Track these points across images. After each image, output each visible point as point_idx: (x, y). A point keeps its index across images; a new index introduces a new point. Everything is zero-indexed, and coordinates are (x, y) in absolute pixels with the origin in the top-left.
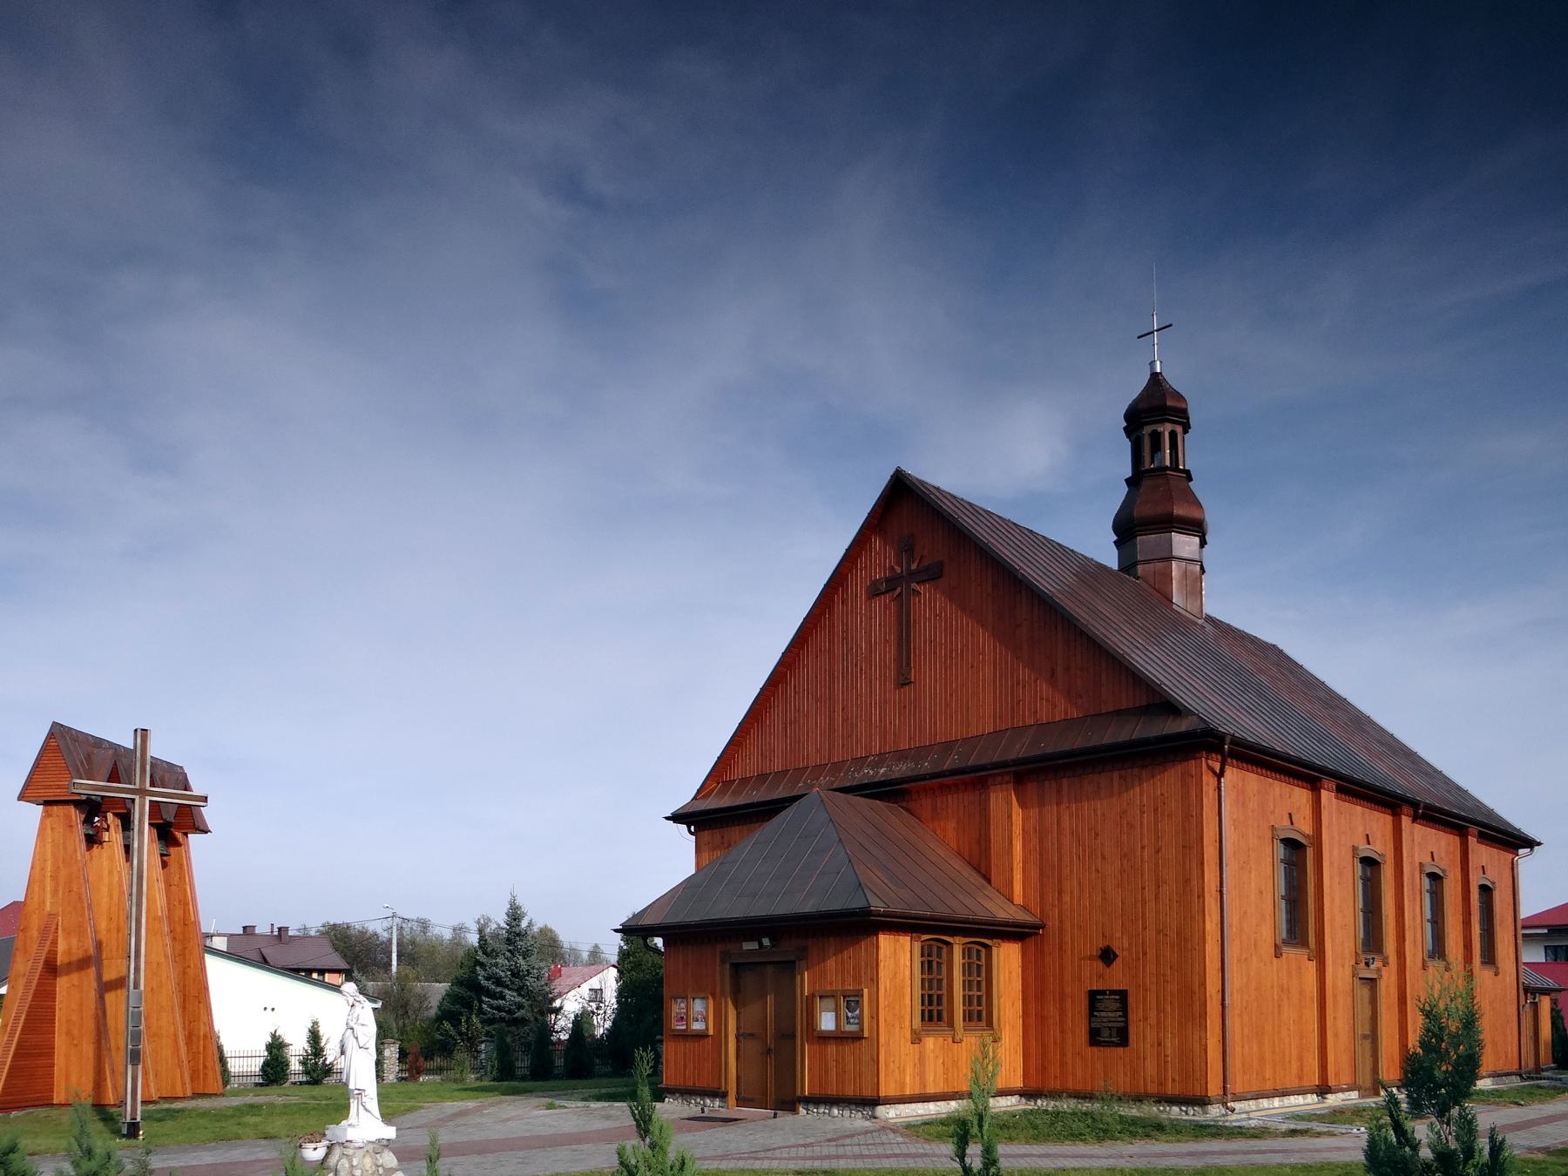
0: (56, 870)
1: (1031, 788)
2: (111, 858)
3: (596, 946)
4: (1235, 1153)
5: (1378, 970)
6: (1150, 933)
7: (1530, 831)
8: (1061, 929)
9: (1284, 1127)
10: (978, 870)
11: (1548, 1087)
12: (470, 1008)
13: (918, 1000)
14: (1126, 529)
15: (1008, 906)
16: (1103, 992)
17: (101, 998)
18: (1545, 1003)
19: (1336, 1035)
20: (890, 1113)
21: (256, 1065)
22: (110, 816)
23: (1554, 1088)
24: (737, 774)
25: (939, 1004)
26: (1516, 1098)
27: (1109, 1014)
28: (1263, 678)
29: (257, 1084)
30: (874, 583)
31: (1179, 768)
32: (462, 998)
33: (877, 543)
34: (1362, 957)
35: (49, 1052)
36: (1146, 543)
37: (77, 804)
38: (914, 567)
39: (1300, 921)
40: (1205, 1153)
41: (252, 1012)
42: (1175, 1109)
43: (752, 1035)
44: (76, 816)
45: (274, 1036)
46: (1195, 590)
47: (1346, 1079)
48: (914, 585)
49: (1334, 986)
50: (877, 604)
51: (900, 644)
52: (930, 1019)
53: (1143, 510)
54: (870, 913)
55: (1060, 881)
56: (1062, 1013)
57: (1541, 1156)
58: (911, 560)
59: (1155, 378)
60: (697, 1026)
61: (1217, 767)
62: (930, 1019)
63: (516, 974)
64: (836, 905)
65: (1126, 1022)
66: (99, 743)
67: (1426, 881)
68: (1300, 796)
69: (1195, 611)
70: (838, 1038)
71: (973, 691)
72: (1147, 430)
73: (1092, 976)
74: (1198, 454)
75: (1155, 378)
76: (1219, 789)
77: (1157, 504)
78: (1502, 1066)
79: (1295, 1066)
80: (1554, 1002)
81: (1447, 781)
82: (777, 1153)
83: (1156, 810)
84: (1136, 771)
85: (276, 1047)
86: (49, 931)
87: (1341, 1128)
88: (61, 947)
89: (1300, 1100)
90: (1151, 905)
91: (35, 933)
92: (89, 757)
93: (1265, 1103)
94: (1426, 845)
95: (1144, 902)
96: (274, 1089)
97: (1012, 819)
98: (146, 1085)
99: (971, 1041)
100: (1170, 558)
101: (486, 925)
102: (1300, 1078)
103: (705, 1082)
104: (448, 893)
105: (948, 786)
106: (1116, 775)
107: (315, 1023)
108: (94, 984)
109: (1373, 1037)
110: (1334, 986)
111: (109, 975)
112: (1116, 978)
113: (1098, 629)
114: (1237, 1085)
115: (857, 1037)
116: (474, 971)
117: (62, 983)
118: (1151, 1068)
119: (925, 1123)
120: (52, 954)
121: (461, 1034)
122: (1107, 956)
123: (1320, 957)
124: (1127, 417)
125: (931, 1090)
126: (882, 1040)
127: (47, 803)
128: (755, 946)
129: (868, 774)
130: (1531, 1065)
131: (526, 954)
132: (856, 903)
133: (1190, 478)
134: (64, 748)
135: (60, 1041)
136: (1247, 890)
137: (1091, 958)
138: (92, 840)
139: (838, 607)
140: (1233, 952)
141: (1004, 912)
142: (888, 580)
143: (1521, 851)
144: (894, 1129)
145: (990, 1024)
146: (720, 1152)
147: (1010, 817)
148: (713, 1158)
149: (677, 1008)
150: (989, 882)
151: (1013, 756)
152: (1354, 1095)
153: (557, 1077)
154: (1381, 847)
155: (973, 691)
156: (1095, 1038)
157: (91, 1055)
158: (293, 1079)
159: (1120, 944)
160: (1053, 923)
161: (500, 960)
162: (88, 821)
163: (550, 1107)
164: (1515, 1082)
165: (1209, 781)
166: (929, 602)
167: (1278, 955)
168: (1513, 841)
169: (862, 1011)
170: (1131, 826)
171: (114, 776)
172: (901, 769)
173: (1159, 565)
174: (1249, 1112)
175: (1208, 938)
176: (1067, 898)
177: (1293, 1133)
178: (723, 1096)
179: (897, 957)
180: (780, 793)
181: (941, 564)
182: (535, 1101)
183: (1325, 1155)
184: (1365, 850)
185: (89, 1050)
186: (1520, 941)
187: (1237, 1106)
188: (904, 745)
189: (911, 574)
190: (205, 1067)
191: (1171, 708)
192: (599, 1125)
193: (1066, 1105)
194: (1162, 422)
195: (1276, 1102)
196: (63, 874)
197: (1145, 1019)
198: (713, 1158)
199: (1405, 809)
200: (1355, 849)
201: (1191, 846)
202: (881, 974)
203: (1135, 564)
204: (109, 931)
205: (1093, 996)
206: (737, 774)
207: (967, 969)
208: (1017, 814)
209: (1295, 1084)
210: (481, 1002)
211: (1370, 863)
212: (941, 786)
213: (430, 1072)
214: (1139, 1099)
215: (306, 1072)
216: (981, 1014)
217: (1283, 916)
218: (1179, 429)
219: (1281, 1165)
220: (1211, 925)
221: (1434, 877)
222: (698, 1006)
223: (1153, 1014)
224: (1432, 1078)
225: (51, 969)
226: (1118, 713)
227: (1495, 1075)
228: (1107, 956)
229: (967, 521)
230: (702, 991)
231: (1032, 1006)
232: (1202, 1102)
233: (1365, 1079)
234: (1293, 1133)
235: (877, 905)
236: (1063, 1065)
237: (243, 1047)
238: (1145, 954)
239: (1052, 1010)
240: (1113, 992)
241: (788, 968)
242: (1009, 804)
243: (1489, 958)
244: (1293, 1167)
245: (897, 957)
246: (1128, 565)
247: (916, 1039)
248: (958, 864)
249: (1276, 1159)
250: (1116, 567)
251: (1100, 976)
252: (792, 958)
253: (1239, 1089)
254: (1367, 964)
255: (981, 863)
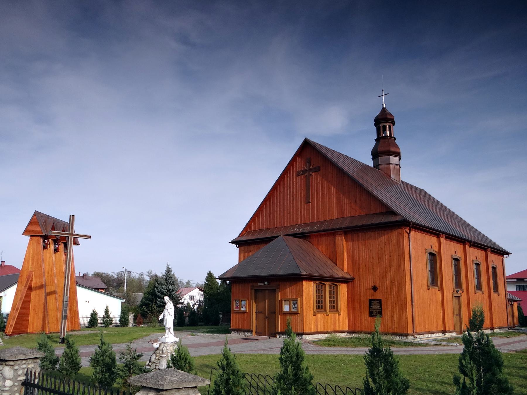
0: (33, 257)
1: (349, 236)
2: (50, 254)
3: (188, 281)
4: (418, 351)
5: (461, 294)
6: (388, 282)
7: (507, 249)
8: (360, 280)
9: (433, 343)
10: (332, 261)
11: (517, 332)
12: (152, 301)
13: (315, 302)
14: (375, 154)
15: (343, 273)
16: (374, 300)
17: (46, 298)
18: (515, 305)
19: (448, 314)
20: (307, 337)
21: (87, 321)
22: (50, 240)
23: (519, 332)
24: (253, 228)
25: (322, 303)
26: (507, 335)
27: (375, 307)
28: (420, 201)
29: (87, 327)
30: (298, 172)
31: (396, 231)
32: (150, 299)
33: (299, 160)
34: (455, 290)
35: (28, 316)
36: (382, 159)
37: (41, 236)
38: (311, 167)
39: (435, 278)
40: (409, 351)
41: (91, 303)
42: (398, 337)
43: (261, 312)
44: (41, 240)
45: (94, 311)
46: (397, 172)
47: (451, 328)
48: (311, 173)
49: (447, 299)
50: (299, 178)
51: (306, 190)
52: (319, 308)
53: (381, 149)
54: (301, 275)
55: (359, 265)
56: (360, 307)
57: (513, 353)
58: (310, 165)
59: (383, 109)
60: (243, 309)
61: (408, 231)
62: (319, 308)
63: (168, 290)
64: (290, 272)
65: (381, 309)
66: (48, 217)
67: (475, 266)
68: (433, 240)
69: (398, 180)
70: (290, 313)
71: (330, 205)
72: (382, 125)
73: (370, 295)
74: (399, 132)
75: (383, 109)
76: (409, 237)
77: (385, 148)
78: (502, 326)
79: (435, 324)
80: (519, 304)
81: (480, 234)
82: (274, 349)
83: (389, 244)
84: (383, 232)
85: (94, 315)
86: (30, 277)
87: (451, 344)
88: (34, 282)
89: (437, 335)
90: (388, 273)
91: (25, 277)
92: (45, 221)
93: (426, 336)
94: (474, 254)
95: (386, 272)
96: (93, 328)
97: (343, 245)
98: (68, 326)
99: (331, 314)
100: (390, 164)
101: (151, 273)
102: (437, 328)
103: (246, 327)
104: (143, 263)
105: (323, 235)
106: (376, 232)
107: (107, 307)
108: (44, 294)
109: (460, 315)
110: (447, 299)
111: (48, 290)
112: (378, 295)
113: (370, 188)
114: (417, 330)
115: (296, 314)
116: (154, 290)
117: (33, 293)
118: (389, 324)
119: (319, 341)
120: (31, 284)
121: (149, 310)
122: (375, 289)
123: (442, 289)
124: (375, 121)
125: (319, 330)
126: (304, 314)
127: (31, 236)
128: (262, 284)
129: (296, 230)
130: (512, 325)
131: (171, 284)
132: (297, 272)
133: (395, 139)
134: (38, 219)
135: (31, 312)
136: (418, 269)
137: (370, 289)
138: (45, 247)
139: (286, 179)
140: (415, 288)
141: (342, 275)
142: (302, 171)
143: (505, 256)
144: (309, 342)
145: (337, 310)
146: (256, 349)
147: (343, 245)
148: (255, 351)
149: (235, 304)
150: (336, 265)
151: (343, 226)
152: (454, 334)
153: (186, 326)
154: (460, 255)
155: (330, 205)
156: (371, 315)
157: (42, 317)
158: (99, 325)
159: (379, 285)
160: (357, 278)
161: (164, 286)
162: (44, 242)
163: (192, 335)
164: (507, 330)
165: (406, 235)
166: (316, 178)
167: (429, 289)
168: (502, 253)
169: (298, 306)
170: (382, 249)
171: (63, 230)
172: (307, 229)
173: (386, 166)
174: (422, 338)
175: (407, 283)
176: (361, 270)
177: (436, 345)
178: (251, 332)
179: (309, 288)
180: (267, 235)
181: (319, 167)
182: (186, 333)
183: (446, 352)
184: (455, 256)
185: (41, 315)
186: (506, 282)
187: (418, 336)
188: (308, 222)
189: (310, 170)
190: (75, 321)
191: (393, 213)
192: (212, 341)
193: (363, 336)
194: (386, 122)
195: (430, 335)
196: (36, 258)
197: (387, 309)
198: (255, 351)
199: (467, 243)
200: (452, 256)
201: (401, 255)
202: (304, 293)
203: (378, 165)
204: (48, 276)
205: (370, 301)
206: (253, 228)
207: (330, 292)
208: (345, 244)
209: (435, 330)
210: (156, 300)
211: (456, 260)
212: (320, 235)
213: (144, 323)
214: (386, 334)
215: (104, 323)
216: (335, 307)
217: (430, 277)
218: (391, 125)
219: (433, 354)
220: (408, 280)
221: (477, 264)
222: (243, 303)
223: (390, 307)
224: (475, 324)
225: (30, 289)
226: (377, 214)
227: (500, 328)
228: (375, 289)
229: (328, 154)
230: (244, 298)
231: (351, 304)
232: (407, 335)
233: (458, 329)
234: (436, 345)
235: (303, 272)
236: (361, 323)
237: (84, 316)
238: (387, 288)
239: (357, 305)
240: (377, 300)
241: (274, 291)
242: (342, 241)
243: (496, 290)
244: (437, 355)
245: (309, 288)
246: (376, 166)
247: (315, 314)
248: (326, 259)
249: (432, 353)
250: (372, 166)
251: (373, 295)
252: (274, 288)
253: (418, 331)
254: (457, 292)
255: (334, 259)
